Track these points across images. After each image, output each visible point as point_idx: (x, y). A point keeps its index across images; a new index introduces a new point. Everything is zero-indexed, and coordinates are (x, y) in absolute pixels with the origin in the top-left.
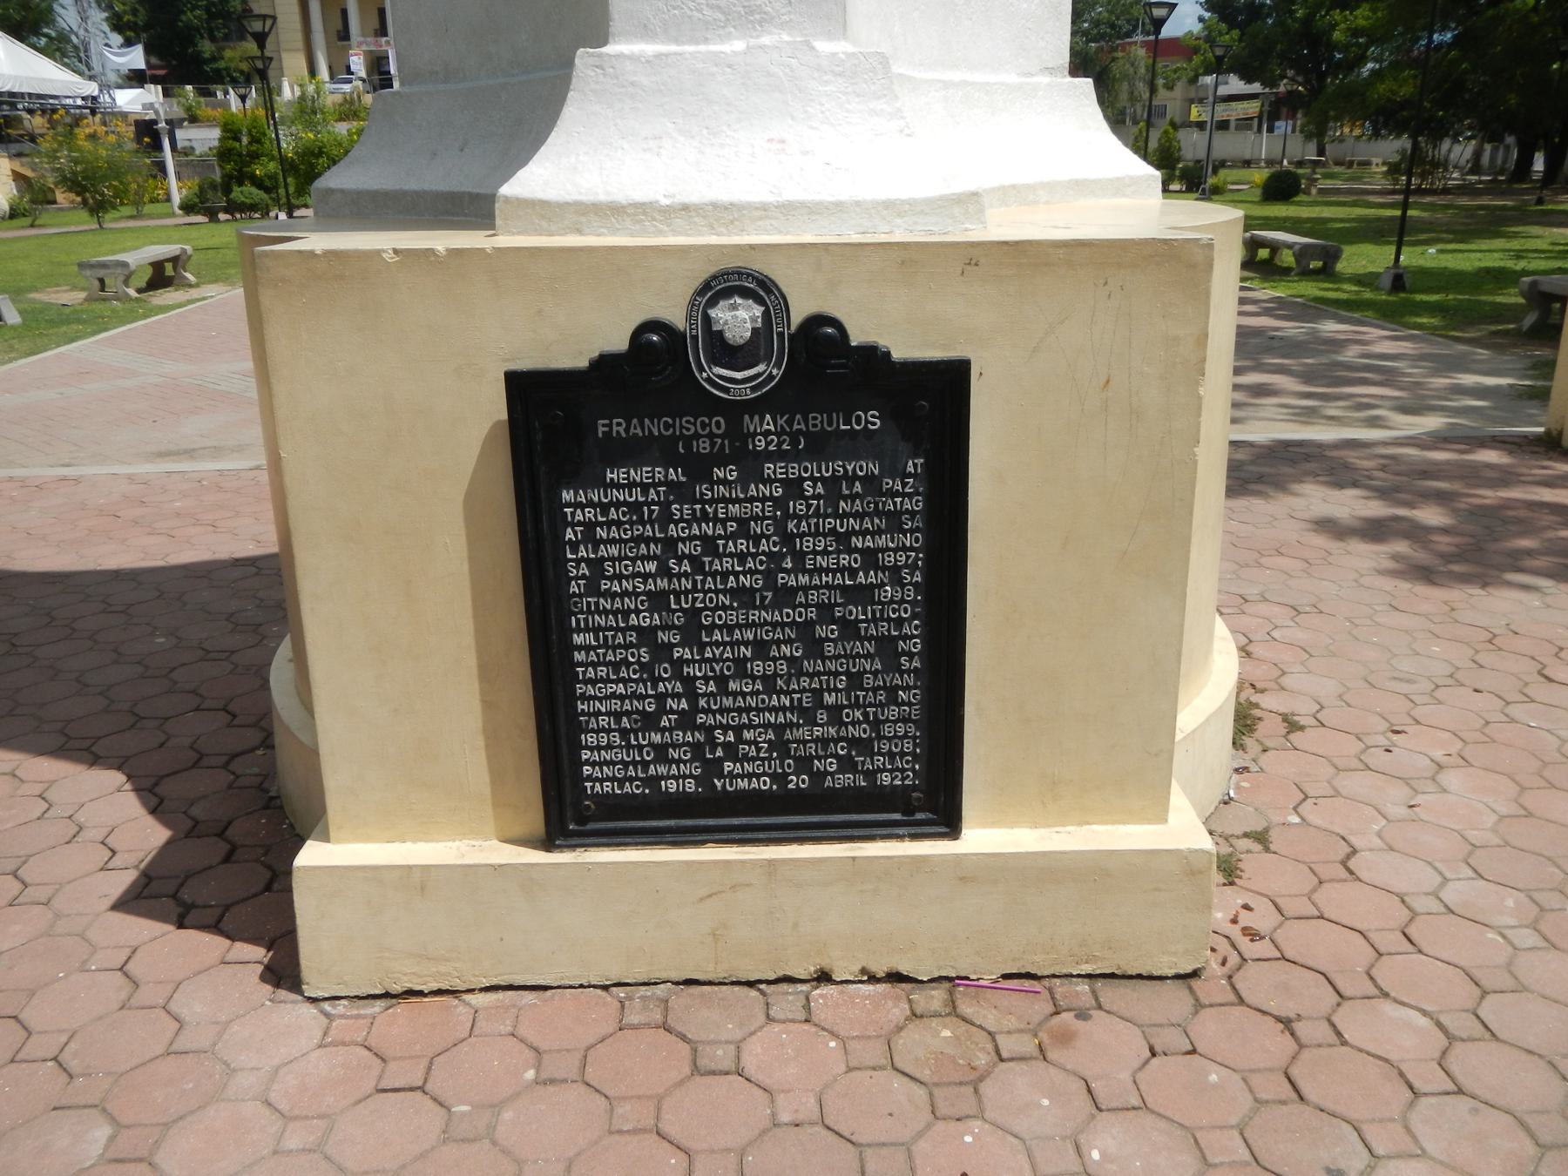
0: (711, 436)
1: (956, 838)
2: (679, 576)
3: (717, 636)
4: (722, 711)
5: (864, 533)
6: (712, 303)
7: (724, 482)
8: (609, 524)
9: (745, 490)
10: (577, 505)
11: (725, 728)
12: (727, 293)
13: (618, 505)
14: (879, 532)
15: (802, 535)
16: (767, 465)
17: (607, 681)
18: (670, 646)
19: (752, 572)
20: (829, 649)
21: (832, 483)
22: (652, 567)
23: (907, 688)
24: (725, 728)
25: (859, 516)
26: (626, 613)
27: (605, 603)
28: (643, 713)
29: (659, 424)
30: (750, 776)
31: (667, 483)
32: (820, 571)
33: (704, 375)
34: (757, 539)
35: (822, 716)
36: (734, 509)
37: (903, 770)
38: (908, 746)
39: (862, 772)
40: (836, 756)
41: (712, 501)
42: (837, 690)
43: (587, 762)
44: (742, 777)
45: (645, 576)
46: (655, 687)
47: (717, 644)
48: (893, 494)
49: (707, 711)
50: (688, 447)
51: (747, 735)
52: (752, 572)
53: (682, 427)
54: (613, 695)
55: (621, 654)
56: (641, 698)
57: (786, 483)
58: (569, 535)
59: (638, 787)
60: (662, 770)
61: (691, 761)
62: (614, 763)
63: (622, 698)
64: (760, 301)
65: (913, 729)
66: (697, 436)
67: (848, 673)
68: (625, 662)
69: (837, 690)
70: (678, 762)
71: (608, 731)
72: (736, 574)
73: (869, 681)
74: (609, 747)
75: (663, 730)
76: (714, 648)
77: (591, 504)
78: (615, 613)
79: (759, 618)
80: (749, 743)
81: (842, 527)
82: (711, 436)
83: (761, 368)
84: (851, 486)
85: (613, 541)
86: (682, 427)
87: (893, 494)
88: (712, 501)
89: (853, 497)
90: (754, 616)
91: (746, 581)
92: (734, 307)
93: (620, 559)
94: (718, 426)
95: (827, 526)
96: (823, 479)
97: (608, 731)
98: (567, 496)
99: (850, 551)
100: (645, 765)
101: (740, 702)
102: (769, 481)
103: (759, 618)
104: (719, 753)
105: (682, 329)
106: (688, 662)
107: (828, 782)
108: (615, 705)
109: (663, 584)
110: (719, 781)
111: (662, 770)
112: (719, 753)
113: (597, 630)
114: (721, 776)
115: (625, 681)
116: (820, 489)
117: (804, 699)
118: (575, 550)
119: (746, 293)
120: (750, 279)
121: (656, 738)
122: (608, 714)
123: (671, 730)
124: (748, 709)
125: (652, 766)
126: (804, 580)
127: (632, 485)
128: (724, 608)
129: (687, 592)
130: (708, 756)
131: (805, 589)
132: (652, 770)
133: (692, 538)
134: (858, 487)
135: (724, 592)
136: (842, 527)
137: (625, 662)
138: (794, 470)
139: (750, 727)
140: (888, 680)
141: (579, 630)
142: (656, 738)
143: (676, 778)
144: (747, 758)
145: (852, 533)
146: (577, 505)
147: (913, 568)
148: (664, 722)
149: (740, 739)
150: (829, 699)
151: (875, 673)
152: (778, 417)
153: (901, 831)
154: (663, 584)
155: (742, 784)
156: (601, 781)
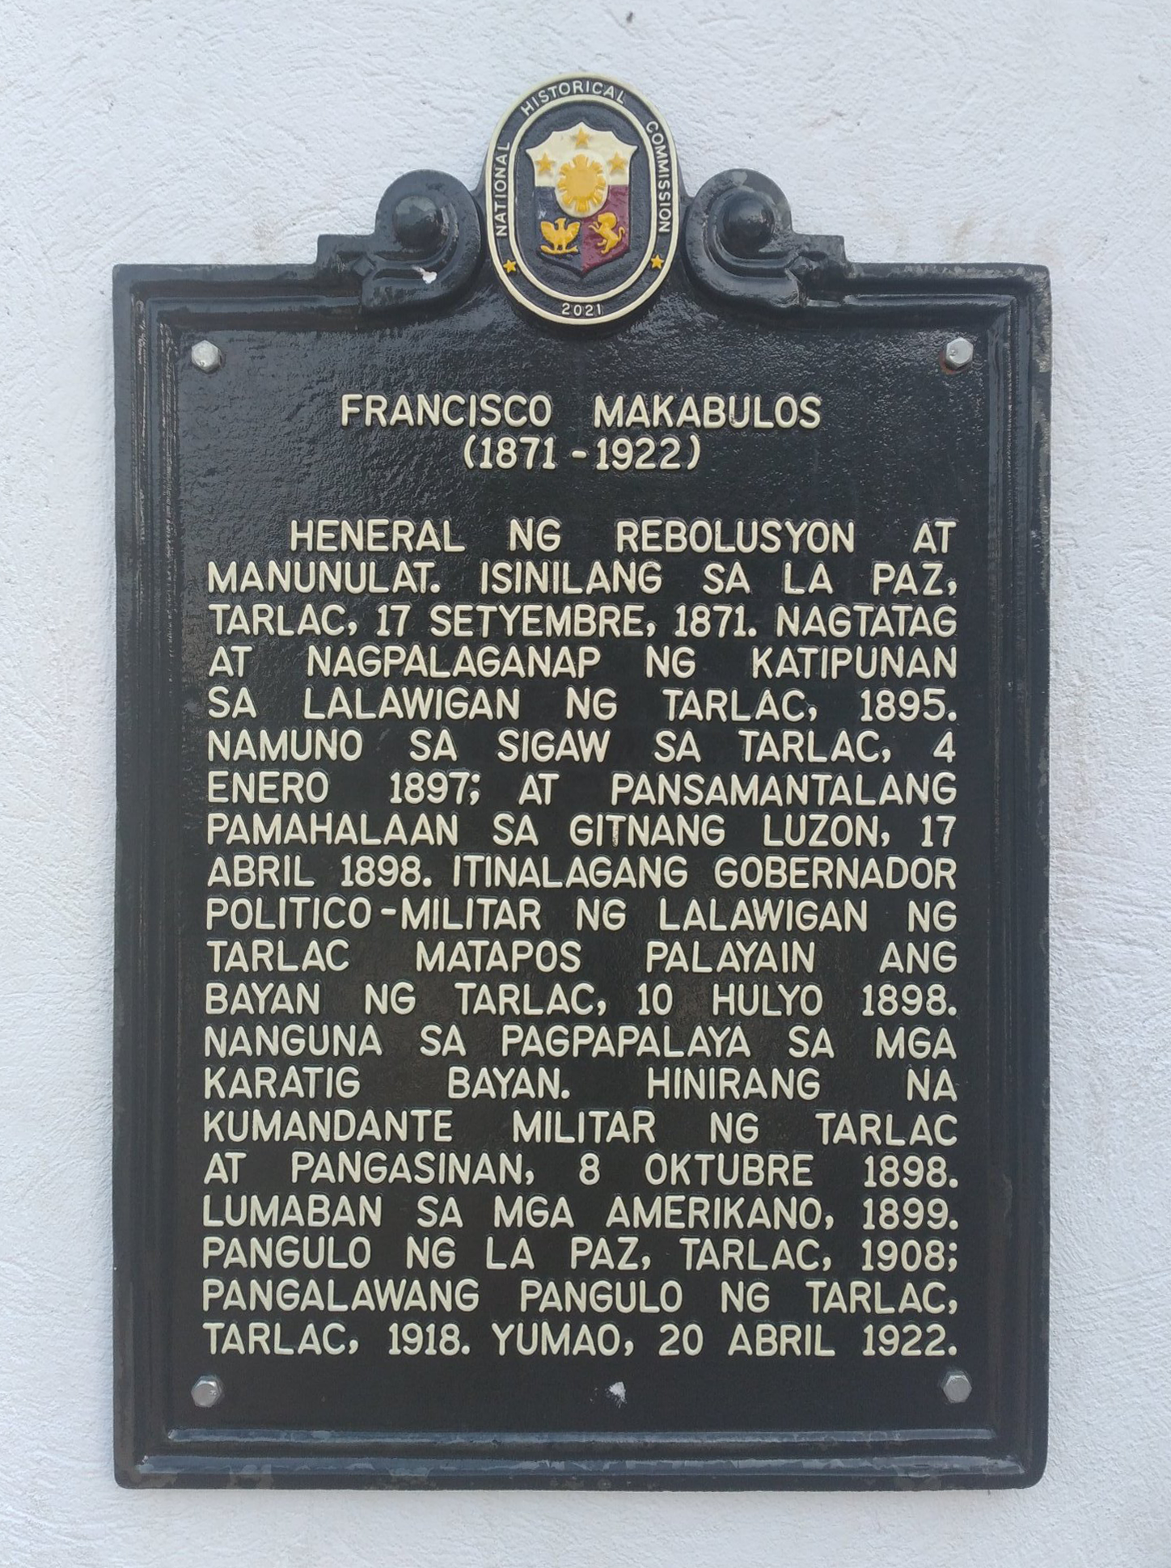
1: (126, 1478)
6: (537, 135)
12: (564, 118)
16: (621, 525)
21: (761, 567)
29: (442, 404)
33: (657, 261)
37: (923, 1319)
39: (821, 1317)
41: (511, 600)
53: (480, 412)
55: (523, 950)
59: (335, 1338)
60: (390, 1295)
61: (454, 1274)
62: (278, 1273)
64: (627, 134)
65: (944, 1214)
70: (426, 1275)
76: (254, 986)
79: (833, 876)
81: (866, 667)
84: (801, 579)
86: (480, 412)
88: (511, 600)
92: (581, 142)
94: (540, 414)
95: (836, 663)
103: (833, 876)
105: (470, 185)
107: (738, 1342)
110: (503, 1329)
117: (439, 1125)
119: (601, 118)
120: (610, 91)
125: (363, 1285)
130: (490, 1265)
136: (866, 667)
138: (680, 535)
140: (504, 1081)
144: (585, 1274)
152: (657, 398)
153: (249, 1468)
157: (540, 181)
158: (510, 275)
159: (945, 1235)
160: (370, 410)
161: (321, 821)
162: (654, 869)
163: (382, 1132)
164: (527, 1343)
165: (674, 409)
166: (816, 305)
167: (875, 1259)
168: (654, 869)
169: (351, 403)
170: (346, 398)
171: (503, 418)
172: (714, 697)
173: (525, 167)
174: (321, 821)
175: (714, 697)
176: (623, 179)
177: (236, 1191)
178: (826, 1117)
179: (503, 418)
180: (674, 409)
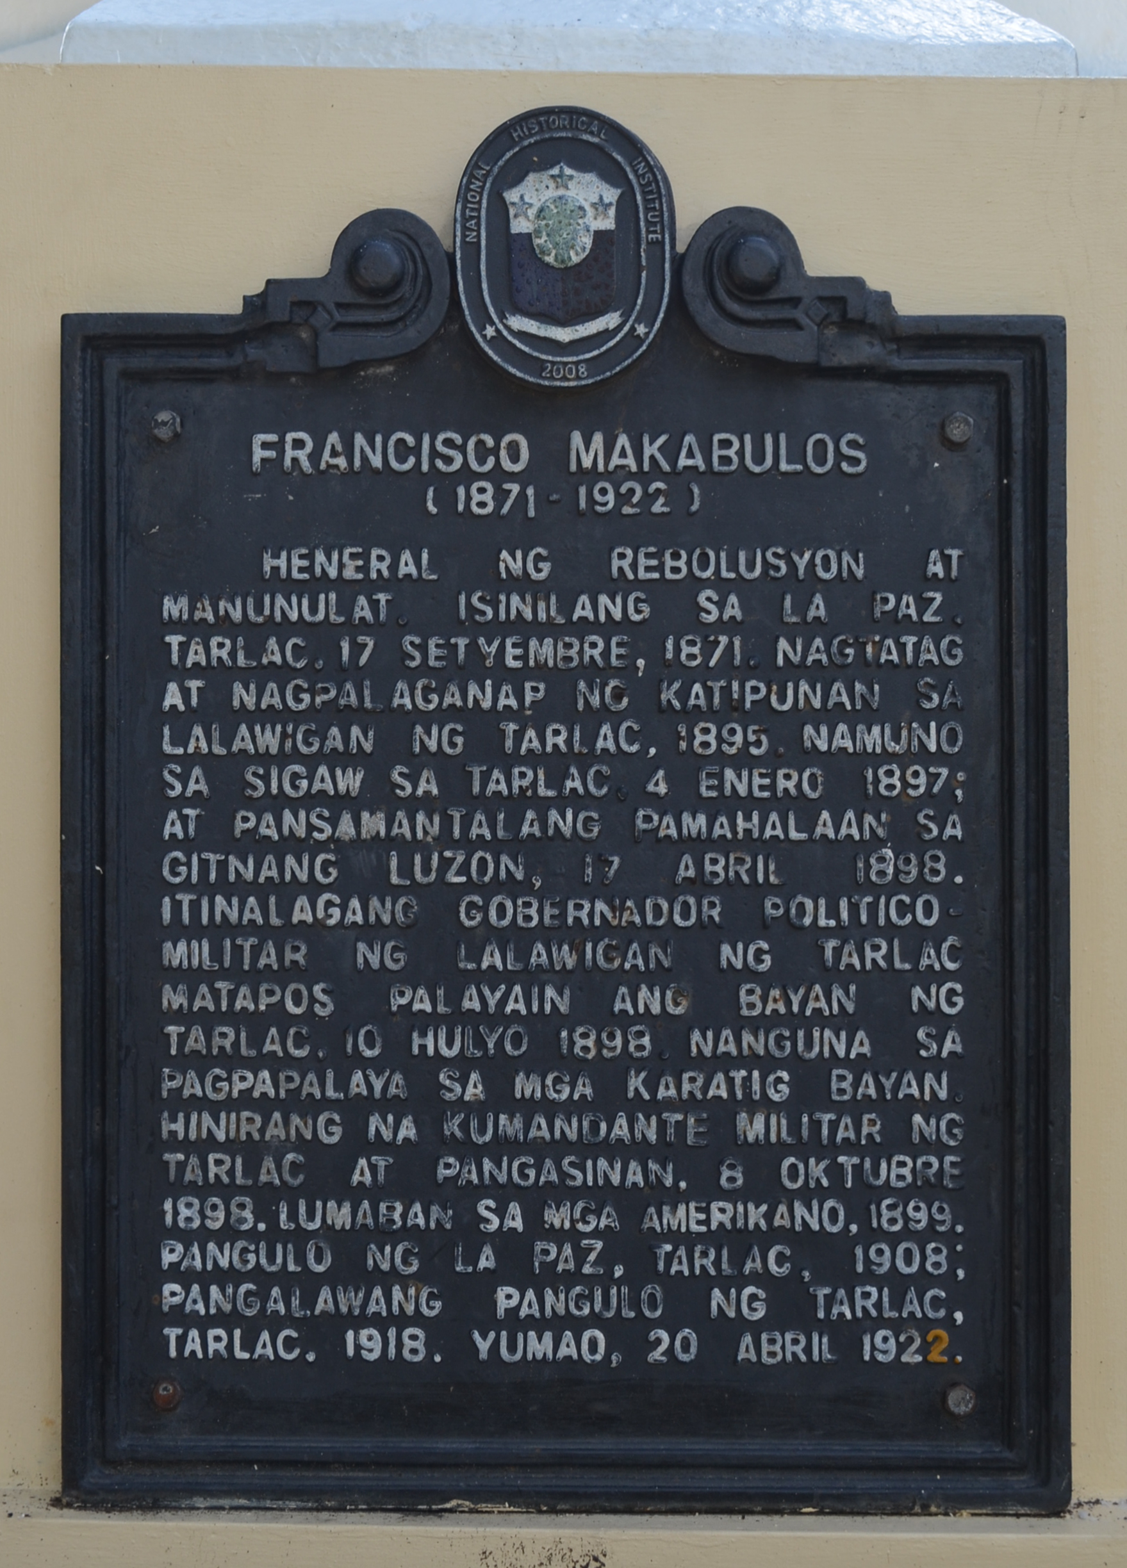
0: (498, 476)
2: (413, 805)
3: (492, 958)
4: (502, 1147)
5: (830, 716)
6: (515, 175)
7: (522, 584)
8: (261, 675)
9: (567, 607)
10: (193, 628)
11: (503, 1194)
13: (283, 629)
14: (866, 716)
15: (693, 715)
17: (231, 1061)
18: (382, 980)
19: (578, 801)
20: (749, 999)
22: (351, 781)
23: (932, 1109)
24: (503, 1194)
25: (821, 675)
26: (287, 891)
27: (241, 868)
28: (310, 1147)
30: (557, 1325)
31: (392, 582)
32: (729, 804)
34: (593, 719)
35: (731, 1176)
36: (545, 650)
37: (925, 1325)
38: (937, 1259)
40: (758, 1279)
42: (767, 1105)
43: (175, 1273)
44: (539, 1324)
45: (338, 803)
46: (342, 1084)
47: (493, 977)
48: (896, 625)
49: (467, 1151)
50: (446, 499)
51: (556, 1217)
52: (578, 801)
54: (246, 1100)
56: (312, 1107)
57: (656, 591)
58: (173, 697)
63: (265, 1106)
64: (612, 174)
66: (467, 475)
67: (794, 1063)
68: (278, 1013)
69: (767, 1105)
71: (226, 1190)
72: (542, 807)
73: (841, 1084)
74: (229, 1234)
75: (355, 1195)
77: (224, 625)
78: (262, 890)
80: (558, 1236)
82: (498, 476)
83: (611, 320)
84: (801, 607)
85: (268, 717)
87: (896, 625)
89: (808, 630)
90: (582, 911)
91: (565, 822)
93: (283, 759)
96: (740, 585)
97: (226, 1190)
98: (173, 608)
99: (806, 757)
100: (309, 1284)
101: (540, 1129)
102: (619, 586)
104: (486, 1260)
106: (425, 1022)
108: (248, 1124)
109: (374, 824)
111: (349, 1301)
112: (486, 1260)
113: (219, 931)
114: (489, 1323)
115: (276, 1064)
116: (734, 609)
118: (180, 739)
121: (341, 1216)
122: (230, 1146)
123: (375, 1193)
124: (558, 1148)
126: (696, 824)
127: (315, 585)
128: (513, 888)
129: (425, 849)
131: (699, 845)
132: (324, 1301)
133: (444, 715)
134: (818, 608)
135: (514, 845)
137: (278, 1013)
139: (562, 1193)
141: (178, 931)
142: (341, 1216)
143: (381, 1323)
144: (550, 1278)
145: (802, 716)
146: (193, 628)
147: (942, 803)
148: (361, 1173)
149: (536, 1226)
150: (753, 1128)
151: (859, 1066)
154: (374, 824)
155: (539, 1346)
156: (203, 1324)
157: (520, 226)
158: (491, 342)
159: (950, 1238)
160: (289, 453)
161: (748, 818)
162: (218, 1124)
163: (207, 1307)
164: (512, 1348)
165: (671, 451)
166: (822, 1309)
167: (867, 1260)
168: (218, 1124)
169: (265, 446)
170: (260, 438)
171: (466, 462)
172: (294, 440)
173: (500, 212)
174: (748, 818)
175: (294, 440)
176: (607, 223)
177: (291, 1195)
178: (823, 1292)
179: (466, 462)
180: (671, 451)
